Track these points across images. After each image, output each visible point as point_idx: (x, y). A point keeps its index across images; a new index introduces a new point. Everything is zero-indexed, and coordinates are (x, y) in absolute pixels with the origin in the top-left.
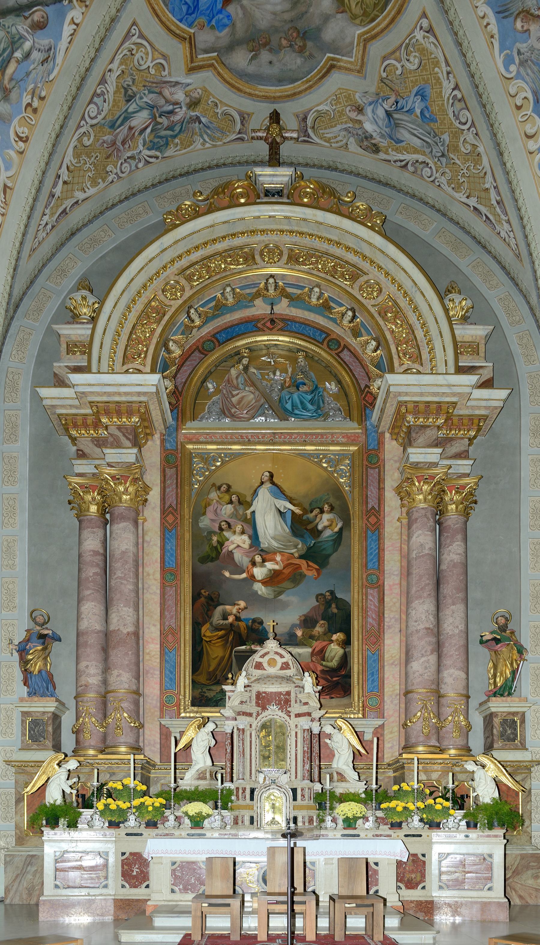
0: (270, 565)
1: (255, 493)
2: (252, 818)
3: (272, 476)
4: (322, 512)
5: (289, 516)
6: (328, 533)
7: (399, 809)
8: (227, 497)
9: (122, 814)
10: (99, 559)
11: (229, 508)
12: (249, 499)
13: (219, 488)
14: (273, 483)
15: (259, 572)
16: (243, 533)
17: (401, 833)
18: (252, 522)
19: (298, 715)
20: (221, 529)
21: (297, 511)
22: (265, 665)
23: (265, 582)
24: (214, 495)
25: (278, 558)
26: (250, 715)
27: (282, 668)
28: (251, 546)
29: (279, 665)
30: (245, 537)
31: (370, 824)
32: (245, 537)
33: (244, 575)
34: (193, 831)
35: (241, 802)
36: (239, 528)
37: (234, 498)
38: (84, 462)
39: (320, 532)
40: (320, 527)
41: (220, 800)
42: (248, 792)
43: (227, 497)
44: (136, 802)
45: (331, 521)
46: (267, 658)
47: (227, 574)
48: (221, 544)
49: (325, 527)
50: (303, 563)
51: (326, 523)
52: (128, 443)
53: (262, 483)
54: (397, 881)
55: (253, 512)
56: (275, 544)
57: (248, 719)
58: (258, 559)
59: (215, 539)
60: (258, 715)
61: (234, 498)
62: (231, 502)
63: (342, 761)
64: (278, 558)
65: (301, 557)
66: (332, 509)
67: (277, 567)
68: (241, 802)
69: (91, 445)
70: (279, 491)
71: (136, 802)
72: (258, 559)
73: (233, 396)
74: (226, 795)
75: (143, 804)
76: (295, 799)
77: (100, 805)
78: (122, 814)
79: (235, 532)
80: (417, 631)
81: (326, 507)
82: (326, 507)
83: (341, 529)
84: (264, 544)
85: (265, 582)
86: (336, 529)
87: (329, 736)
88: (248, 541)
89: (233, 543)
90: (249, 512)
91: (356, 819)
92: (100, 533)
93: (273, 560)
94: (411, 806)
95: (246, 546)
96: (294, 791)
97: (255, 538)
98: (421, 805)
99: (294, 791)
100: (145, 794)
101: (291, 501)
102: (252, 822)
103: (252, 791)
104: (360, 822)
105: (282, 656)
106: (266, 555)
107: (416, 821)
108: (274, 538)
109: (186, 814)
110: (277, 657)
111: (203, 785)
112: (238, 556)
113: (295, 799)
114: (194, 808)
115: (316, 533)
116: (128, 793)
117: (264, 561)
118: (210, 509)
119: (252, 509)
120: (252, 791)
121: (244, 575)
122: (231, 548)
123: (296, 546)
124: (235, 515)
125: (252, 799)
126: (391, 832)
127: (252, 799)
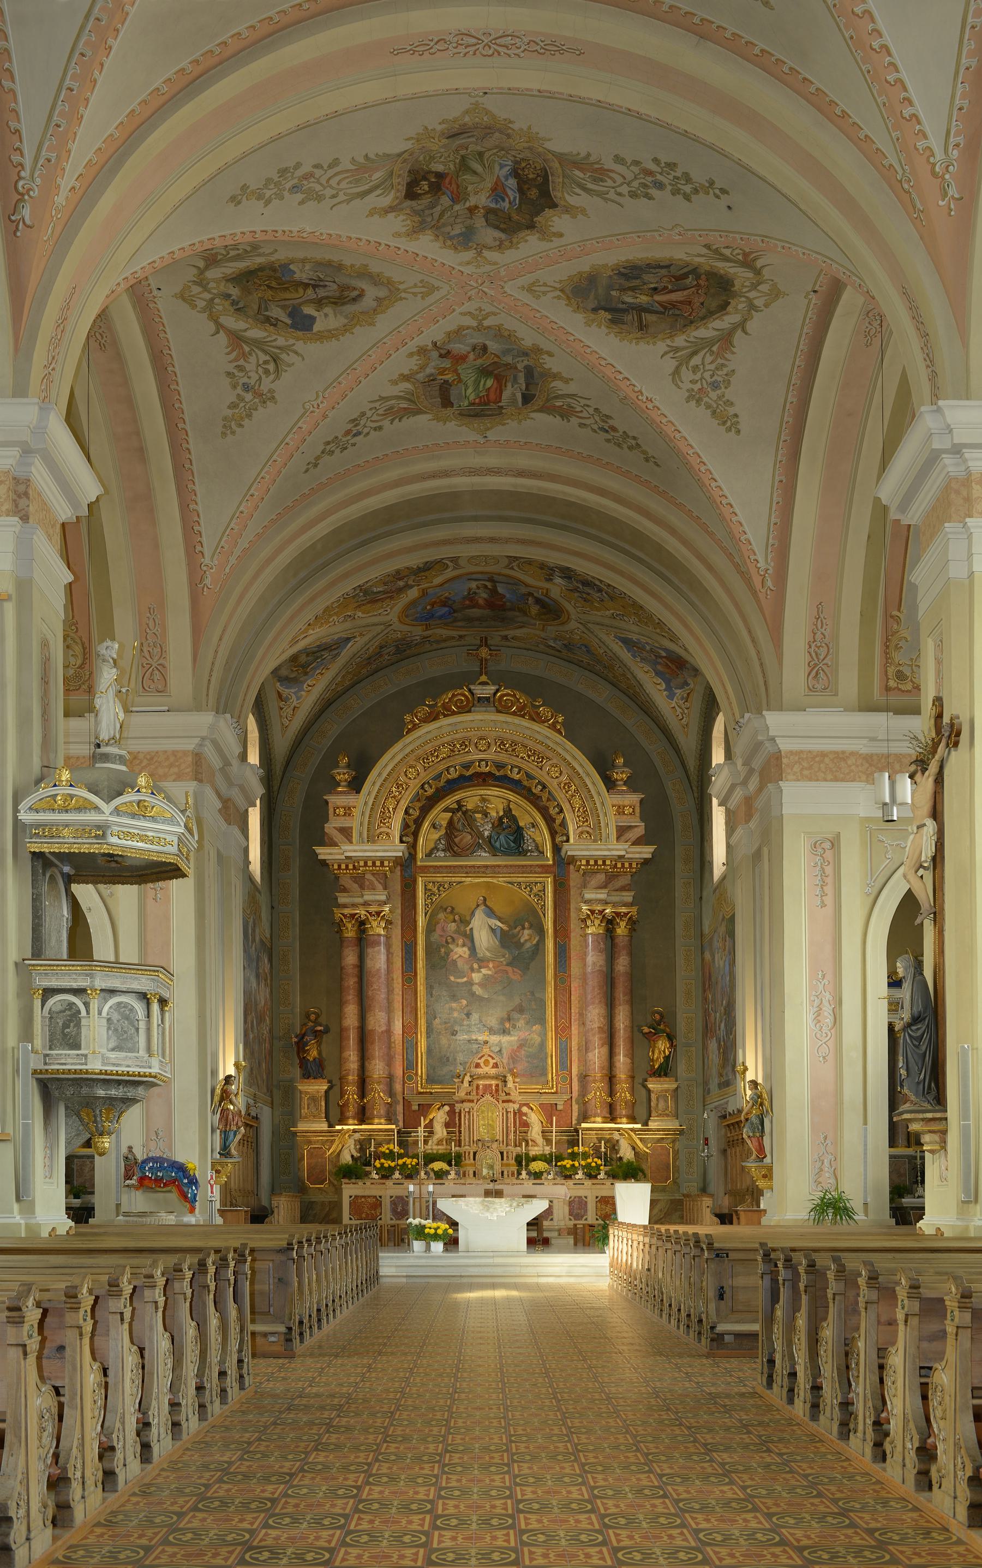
0: (484, 971)
1: (473, 914)
2: (474, 1172)
3: (485, 899)
4: (523, 928)
5: (498, 932)
6: (528, 945)
7: (568, 1166)
8: (451, 917)
9: (391, 1170)
10: (356, 971)
11: (453, 926)
12: (468, 918)
13: (446, 909)
14: (486, 906)
15: (476, 977)
16: (464, 945)
17: (570, 1182)
18: (470, 937)
19: (503, 1102)
20: (447, 942)
21: (505, 928)
22: (482, 1065)
23: (480, 985)
24: (441, 915)
25: (491, 965)
26: (473, 1101)
27: (493, 1067)
28: (470, 956)
29: (491, 1065)
30: (465, 949)
31: (550, 1177)
32: (465, 949)
33: (465, 979)
34: (437, 1181)
35: (467, 1162)
36: (460, 942)
37: (457, 917)
38: (345, 894)
39: (523, 944)
40: (522, 941)
41: (455, 1160)
42: (472, 1154)
43: (451, 917)
44: (400, 1162)
45: (530, 935)
46: (483, 1059)
47: (452, 978)
48: (447, 954)
49: (526, 941)
50: (509, 969)
51: (527, 937)
52: (380, 887)
53: (478, 906)
54: (613, 1198)
55: (472, 929)
56: (488, 954)
57: (471, 1104)
58: (476, 966)
59: (443, 950)
60: (478, 1100)
61: (457, 917)
62: (454, 921)
63: (535, 1132)
64: (491, 965)
65: (507, 965)
66: (531, 927)
67: (490, 973)
68: (467, 1162)
69: (350, 882)
70: (491, 913)
71: (400, 1162)
72: (476, 966)
73: (456, 837)
74: (459, 1157)
75: (404, 1163)
76: (502, 1159)
77: (377, 1164)
78: (391, 1170)
79: (457, 945)
80: (592, 1029)
81: (527, 925)
82: (527, 925)
83: (538, 942)
84: (480, 955)
85: (480, 985)
86: (535, 942)
87: (526, 1114)
88: (468, 952)
89: (456, 953)
90: (468, 929)
91: (541, 1173)
92: (356, 949)
93: (487, 967)
94: (577, 1164)
95: (466, 956)
96: (502, 1153)
97: (473, 949)
98: (583, 1163)
99: (502, 1153)
100: (406, 1155)
101: (500, 920)
102: (474, 1175)
103: (475, 1154)
104: (545, 1175)
105: (493, 1058)
106: (482, 962)
107: (580, 1175)
108: (487, 949)
109: (433, 1170)
110: (490, 1059)
111: (442, 1149)
112: (460, 963)
113: (502, 1159)
114: (437, 1165)
115: (519, 945)
116: (391, 1155)
117: (480, 967)
118: (439, 927)
119: (470, 926)
120: (475, 1154)
121: (465, 979)
122: (455, 957)
123: (504, 956)
124: (457, 931)
125: (474, 1159)
126: (563, 1181)
127: (474, 1159)
